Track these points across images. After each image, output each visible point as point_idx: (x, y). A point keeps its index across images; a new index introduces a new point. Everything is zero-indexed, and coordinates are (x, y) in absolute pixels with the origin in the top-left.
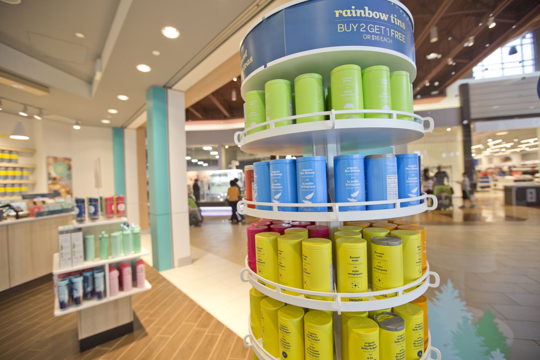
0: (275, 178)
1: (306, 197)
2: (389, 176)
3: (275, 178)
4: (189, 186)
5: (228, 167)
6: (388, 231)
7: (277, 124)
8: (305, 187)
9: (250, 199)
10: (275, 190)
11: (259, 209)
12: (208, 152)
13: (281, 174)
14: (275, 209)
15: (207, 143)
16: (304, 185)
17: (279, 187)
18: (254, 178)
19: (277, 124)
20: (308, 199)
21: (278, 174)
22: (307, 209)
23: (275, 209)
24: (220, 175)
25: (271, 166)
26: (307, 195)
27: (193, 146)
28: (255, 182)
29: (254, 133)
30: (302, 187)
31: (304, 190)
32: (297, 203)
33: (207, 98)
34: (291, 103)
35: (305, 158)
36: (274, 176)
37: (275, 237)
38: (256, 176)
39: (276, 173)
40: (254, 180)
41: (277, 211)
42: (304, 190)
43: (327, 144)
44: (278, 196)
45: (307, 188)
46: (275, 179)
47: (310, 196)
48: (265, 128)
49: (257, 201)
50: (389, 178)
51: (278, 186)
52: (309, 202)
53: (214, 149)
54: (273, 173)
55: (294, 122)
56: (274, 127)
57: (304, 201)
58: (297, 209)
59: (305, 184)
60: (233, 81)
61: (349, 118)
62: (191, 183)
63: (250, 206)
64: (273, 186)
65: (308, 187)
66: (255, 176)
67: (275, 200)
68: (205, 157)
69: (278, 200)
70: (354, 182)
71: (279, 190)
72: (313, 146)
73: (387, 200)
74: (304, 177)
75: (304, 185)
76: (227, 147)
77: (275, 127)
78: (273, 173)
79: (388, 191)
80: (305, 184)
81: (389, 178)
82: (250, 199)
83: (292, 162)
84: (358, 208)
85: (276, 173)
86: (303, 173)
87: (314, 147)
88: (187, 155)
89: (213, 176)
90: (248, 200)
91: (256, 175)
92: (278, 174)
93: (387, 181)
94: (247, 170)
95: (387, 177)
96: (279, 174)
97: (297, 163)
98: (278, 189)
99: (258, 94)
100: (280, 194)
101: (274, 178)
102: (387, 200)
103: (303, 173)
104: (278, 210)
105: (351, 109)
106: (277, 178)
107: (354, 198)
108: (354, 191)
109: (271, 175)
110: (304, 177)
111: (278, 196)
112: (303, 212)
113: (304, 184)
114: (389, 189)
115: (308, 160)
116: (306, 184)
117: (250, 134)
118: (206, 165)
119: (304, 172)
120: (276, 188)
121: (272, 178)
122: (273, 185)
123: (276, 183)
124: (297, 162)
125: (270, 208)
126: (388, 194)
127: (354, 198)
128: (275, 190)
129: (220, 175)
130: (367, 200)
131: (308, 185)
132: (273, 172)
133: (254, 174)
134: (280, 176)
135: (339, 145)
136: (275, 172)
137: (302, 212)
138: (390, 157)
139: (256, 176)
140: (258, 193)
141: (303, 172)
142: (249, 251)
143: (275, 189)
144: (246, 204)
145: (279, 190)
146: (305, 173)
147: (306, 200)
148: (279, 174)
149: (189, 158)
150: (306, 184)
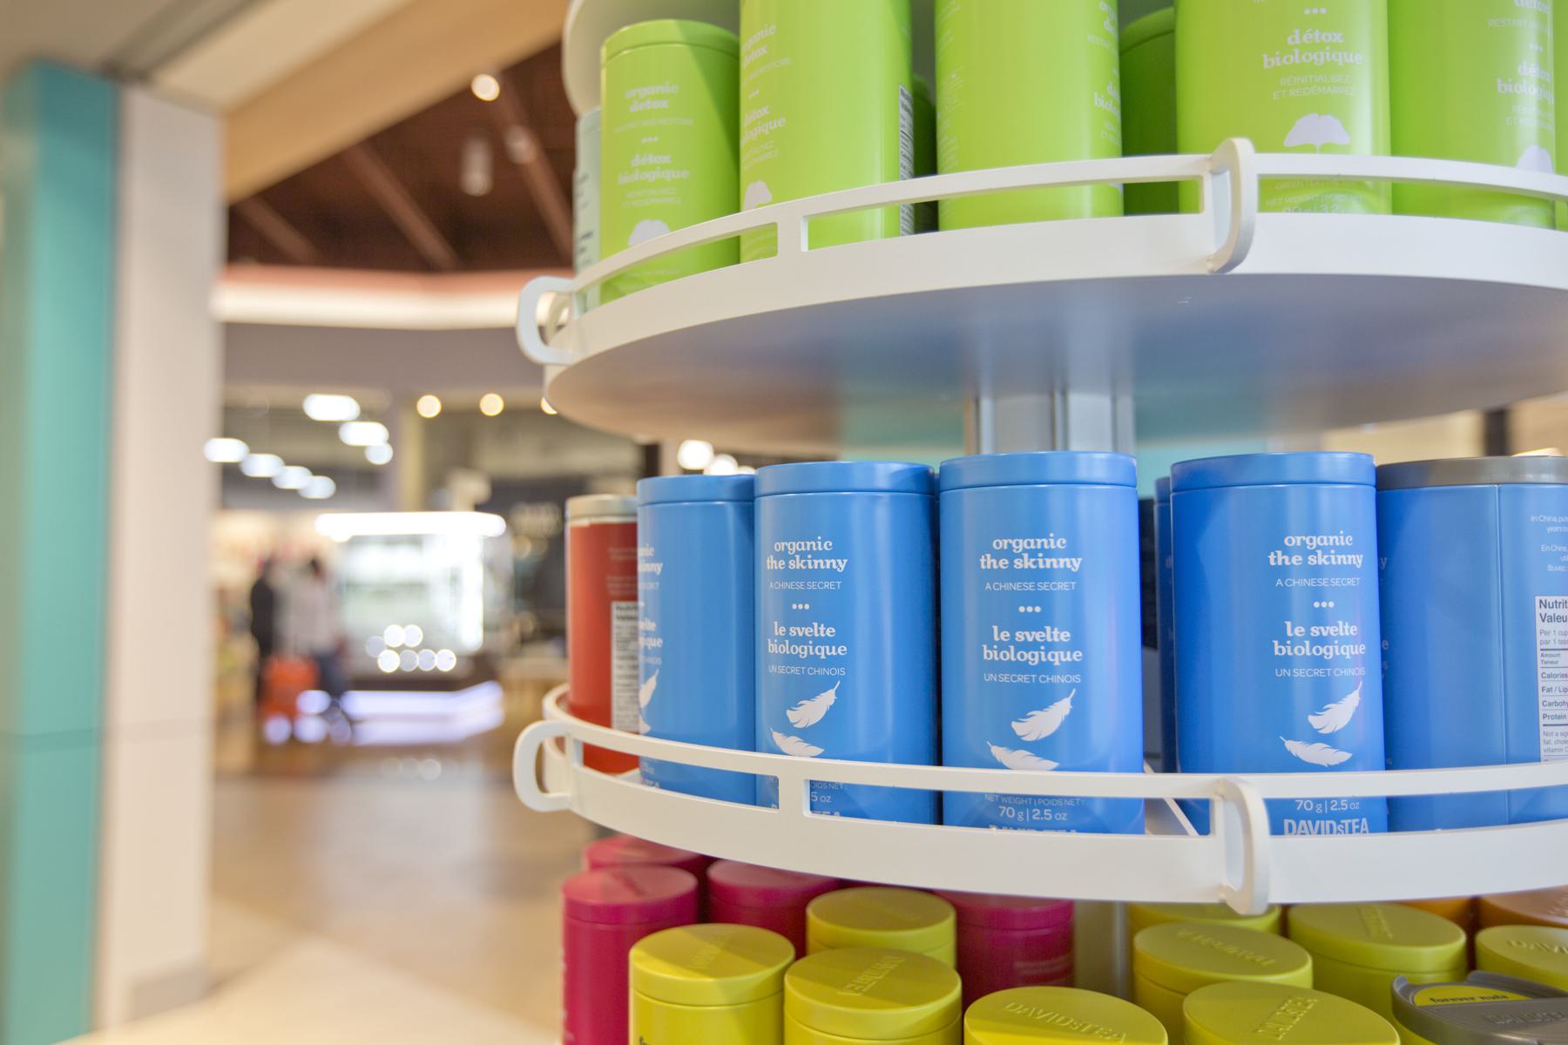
0: (800, 586)
1: (1019, 728)
2: (1551, 599)
3: (800, 586)
4: (222, 595)
5: (433, 497)
6: (1454, 938)
7: (823, 229)
8: (1011, 655)
9: (595, 709)
10: (794, 670)
11: (663, 786)
12: (331, 429)
13: (841, 565)
14: (794, 795)
15: (332, 381)
16: (1003, 646)
17: (823, 652)
18: (640, 578)
19: (823, 229)
20: (1030, 738)
21: (819, 563)
22: (1018, 808)
23: (794, 795)
24: (391, 541)
25: (767, 510)
26: (1022, 715)
27: (260, 395)
28: (641, 604)
29: (650, 286)
30: (989, 654)
31: (1005, 678)
32: (938, 760)
33: (334, 165)
34: (910, 107)
35: (846, 469)
36: (788, 574)
37: (768, 972)
38: (657, 568)
39: (803, 555)
40: (635, 589)
41: (807, 813)
42: (1005, 678)
43: (1064, 394)
44: (812, 711)
45: (1023, 667)
46: (801, 596)
47: (1045, 722)
48: (731, 251)
49: (648, 735)
50: (1550, 612)
51: (818, 641)
52: (1034, 760)
53: (367, 415)
54: (785, 556)
55: (927, 217)
56: (805, 248)
57: (999, 752)
58: (937, 808)
59: (1012, 640)
60: (464, 95)
61: (1320, 210)
62: (239, 576)
63: (599, 759)
64: (781, 640)
65: (1032, 658)
66: (647, 565)
67: (794, 739)
68: (318, 450)
69: (808, 735)
70: (1331, 630)
71: (822, 671)
72: (977, 402)
73: (1539, 760)
74: (1008, 586)
75: (1003, 646)
76: (430, 406)
77: (810, 248)
78: (785, 556)
79: (1542, 697)
80: (1012, 640)
81: (1550, 612)
82: (595, 709)
83: (912, 486)
84: (1356, 806)
85: (803, 555)
86: (1004, 563)
87: (986, 405)
88: (227, 432)
89: (356, 542)
90: (579, 712)
91: (649, 560)
92: (819, 563)
93: (1539, 637)
94: (585, 522)
95: (1539, 611)
96: (830, 563)
97: (947, 499)
98: (814, 661)
99: (690, 44)
100: (828, 698)
101: (785, 585)
102: (1534, 758)
103: (1004, 563)
104: (812, 809)
105: (1326, 149)
106: (812, 586)
107: (1330, 740)
108: (1324, 695)
109: (770, 563)
110: (1008, 586)
111: (812, 711)
112: (994, 830)
113: (1005, 636)
114: (1548, 685)
115: (1023, 478)
116: (1020, 636)
117: (622, 295)
118: (321, 487)
119: (1009, 554)
120: (803, 651)
121: (768, 590)
122: (781, 631)
123: (804, 620)
124: (944, 485)
125: (755, 791)
126: (1542, 722)
127: (1330, 740)
128: (794, 670)
129: (391, 541)
130: (1393, 759)
131: (1034, 646)
132: (780, 546)
133: (643, 551)
134: (831, 574)
135: (1127, 405)
136: (794, 547)
137: (986, 826)
138: (1546, 477)
139: (657, 568)
140: (661, 682)
141: (998, 555)
142: (571, 1036)
143: (791, 660)
144: (576, 741)
145: (822, 671)
146: (1018, 564)
147: (1016, 743)
148: (830, 563)
149: (229, 450)
150: (1020, 636)
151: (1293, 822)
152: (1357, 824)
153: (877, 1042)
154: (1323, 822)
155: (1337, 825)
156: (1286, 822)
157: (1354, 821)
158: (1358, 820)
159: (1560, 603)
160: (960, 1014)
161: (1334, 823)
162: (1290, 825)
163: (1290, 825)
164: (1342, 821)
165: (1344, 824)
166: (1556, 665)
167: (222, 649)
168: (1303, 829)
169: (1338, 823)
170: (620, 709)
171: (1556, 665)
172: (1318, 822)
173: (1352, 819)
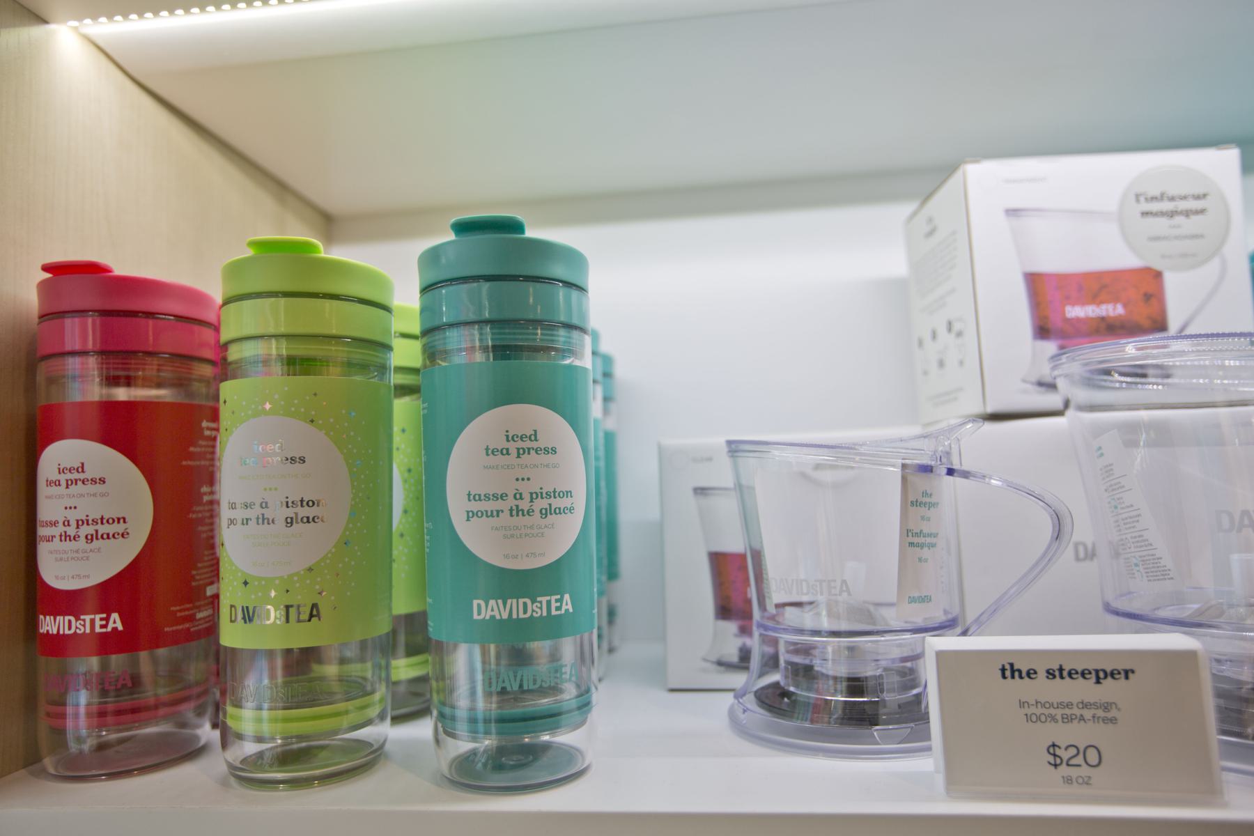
151: (482, 603)
152: (557, 601)
153: (90, 773)
154: (515, 601)
155: (533, 604)
156: (475, 602)
157: (98, 617)
158: (104, 616)
159: (1099, 717)
160: (909, 626)
161: (528, 601)
162: (479, 605)
163: (479, 605)
164: (539, 599)
165: (84, 620)
166: (1123, 489)
167: (221, 465)
168: (492, 610)
169: (533, 601)
170: (50, 483)
171: (1123, 489)
172: (509, 601)
173: (551, 595)
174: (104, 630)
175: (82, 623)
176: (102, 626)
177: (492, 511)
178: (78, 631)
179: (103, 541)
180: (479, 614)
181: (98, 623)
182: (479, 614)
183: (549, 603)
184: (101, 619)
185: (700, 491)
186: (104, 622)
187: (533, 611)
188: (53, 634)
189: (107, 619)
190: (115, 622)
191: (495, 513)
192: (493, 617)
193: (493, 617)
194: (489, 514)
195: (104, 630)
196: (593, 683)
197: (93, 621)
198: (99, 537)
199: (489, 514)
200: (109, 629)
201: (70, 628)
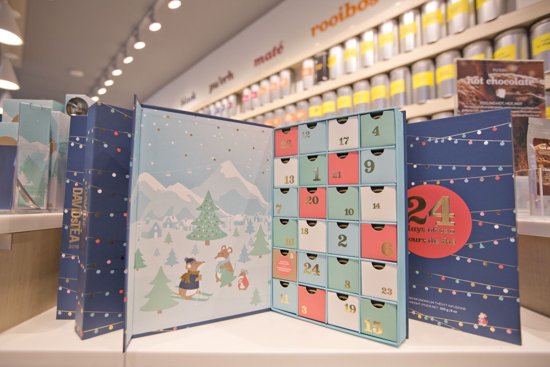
165: (78, 223)
174: (71, 233)
175: (76, 222)
176: (73, 232)
177: (417, 239)
178: (72, 219)
179: (418, 227)
180: (76, 191)
181: (75, 230)
182: (76, 191)
183: (77, 227)
184: (77, 232)
185: (311, 256)
186: (75, 233)
187: (74, 219)
188: (71, 202)
189: (77, 235)
190: (74, 239)
191: (418, 240)
192: (73, 198)
193: (73, 198)
194: (415, 240)
195: (71, 233)
196: (19, 184)
197: (77, 227)
198: (410, 229)
199: (415, 240)
200: (71, 236)
201: (74, 214)
